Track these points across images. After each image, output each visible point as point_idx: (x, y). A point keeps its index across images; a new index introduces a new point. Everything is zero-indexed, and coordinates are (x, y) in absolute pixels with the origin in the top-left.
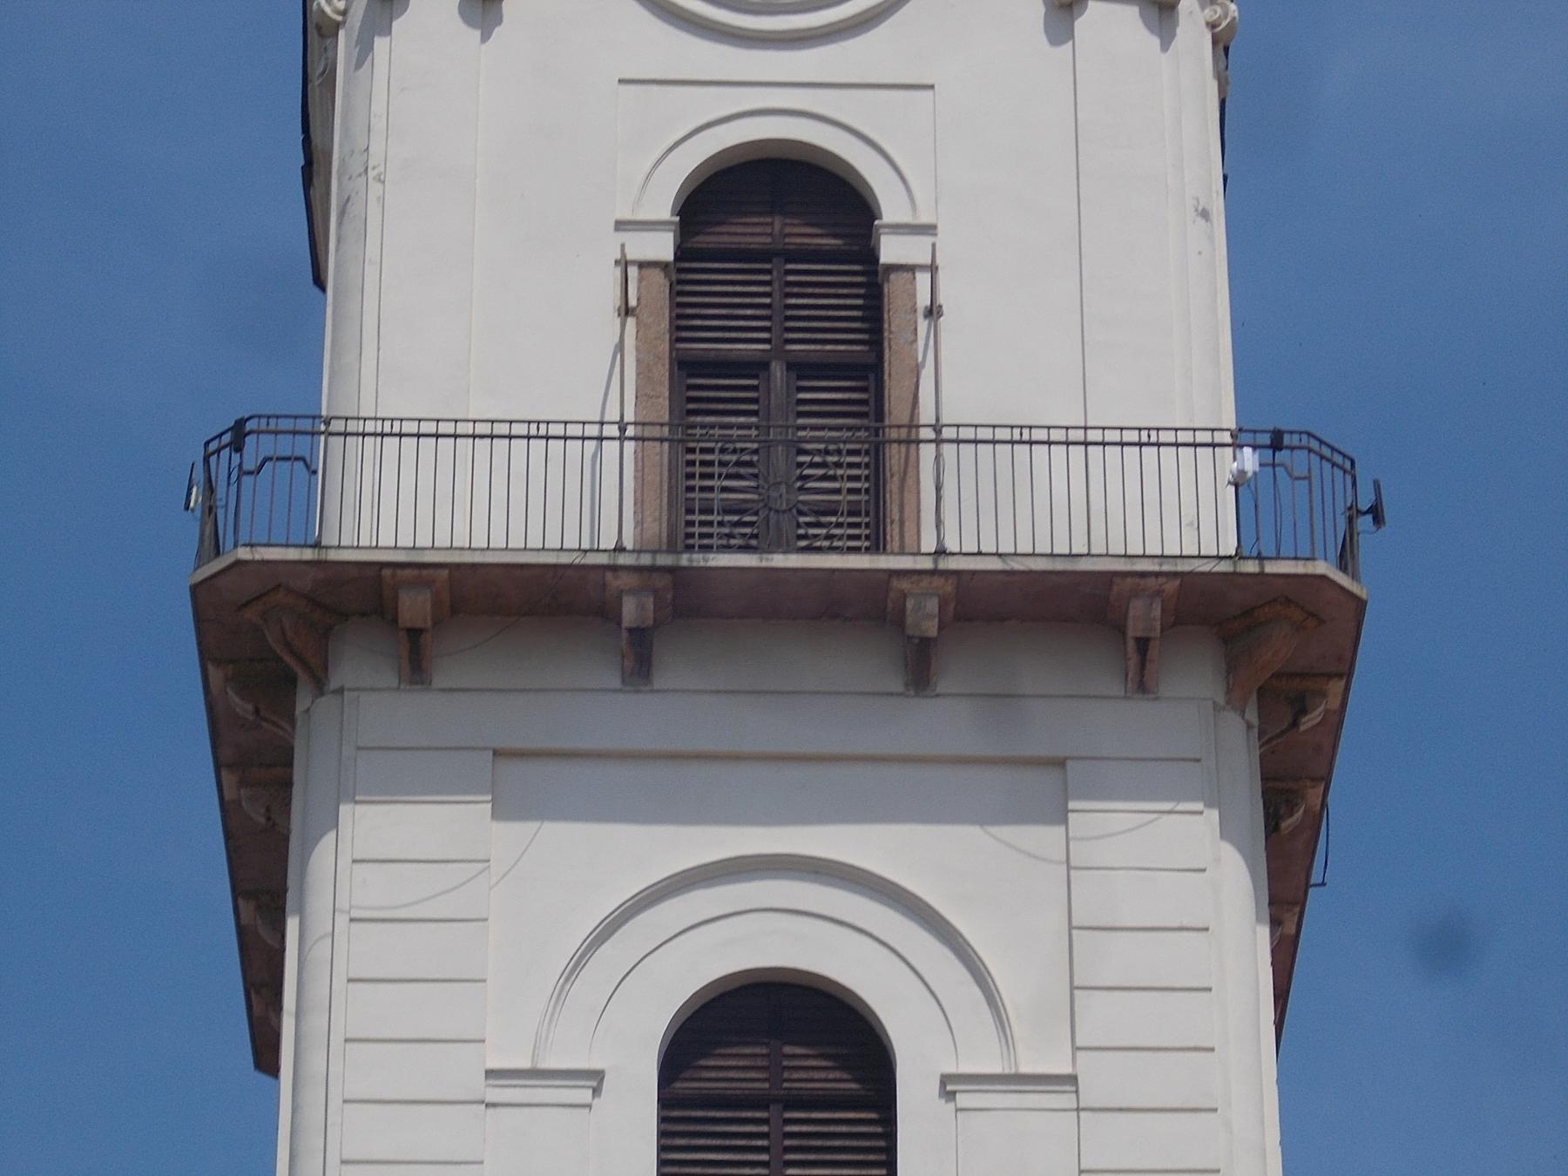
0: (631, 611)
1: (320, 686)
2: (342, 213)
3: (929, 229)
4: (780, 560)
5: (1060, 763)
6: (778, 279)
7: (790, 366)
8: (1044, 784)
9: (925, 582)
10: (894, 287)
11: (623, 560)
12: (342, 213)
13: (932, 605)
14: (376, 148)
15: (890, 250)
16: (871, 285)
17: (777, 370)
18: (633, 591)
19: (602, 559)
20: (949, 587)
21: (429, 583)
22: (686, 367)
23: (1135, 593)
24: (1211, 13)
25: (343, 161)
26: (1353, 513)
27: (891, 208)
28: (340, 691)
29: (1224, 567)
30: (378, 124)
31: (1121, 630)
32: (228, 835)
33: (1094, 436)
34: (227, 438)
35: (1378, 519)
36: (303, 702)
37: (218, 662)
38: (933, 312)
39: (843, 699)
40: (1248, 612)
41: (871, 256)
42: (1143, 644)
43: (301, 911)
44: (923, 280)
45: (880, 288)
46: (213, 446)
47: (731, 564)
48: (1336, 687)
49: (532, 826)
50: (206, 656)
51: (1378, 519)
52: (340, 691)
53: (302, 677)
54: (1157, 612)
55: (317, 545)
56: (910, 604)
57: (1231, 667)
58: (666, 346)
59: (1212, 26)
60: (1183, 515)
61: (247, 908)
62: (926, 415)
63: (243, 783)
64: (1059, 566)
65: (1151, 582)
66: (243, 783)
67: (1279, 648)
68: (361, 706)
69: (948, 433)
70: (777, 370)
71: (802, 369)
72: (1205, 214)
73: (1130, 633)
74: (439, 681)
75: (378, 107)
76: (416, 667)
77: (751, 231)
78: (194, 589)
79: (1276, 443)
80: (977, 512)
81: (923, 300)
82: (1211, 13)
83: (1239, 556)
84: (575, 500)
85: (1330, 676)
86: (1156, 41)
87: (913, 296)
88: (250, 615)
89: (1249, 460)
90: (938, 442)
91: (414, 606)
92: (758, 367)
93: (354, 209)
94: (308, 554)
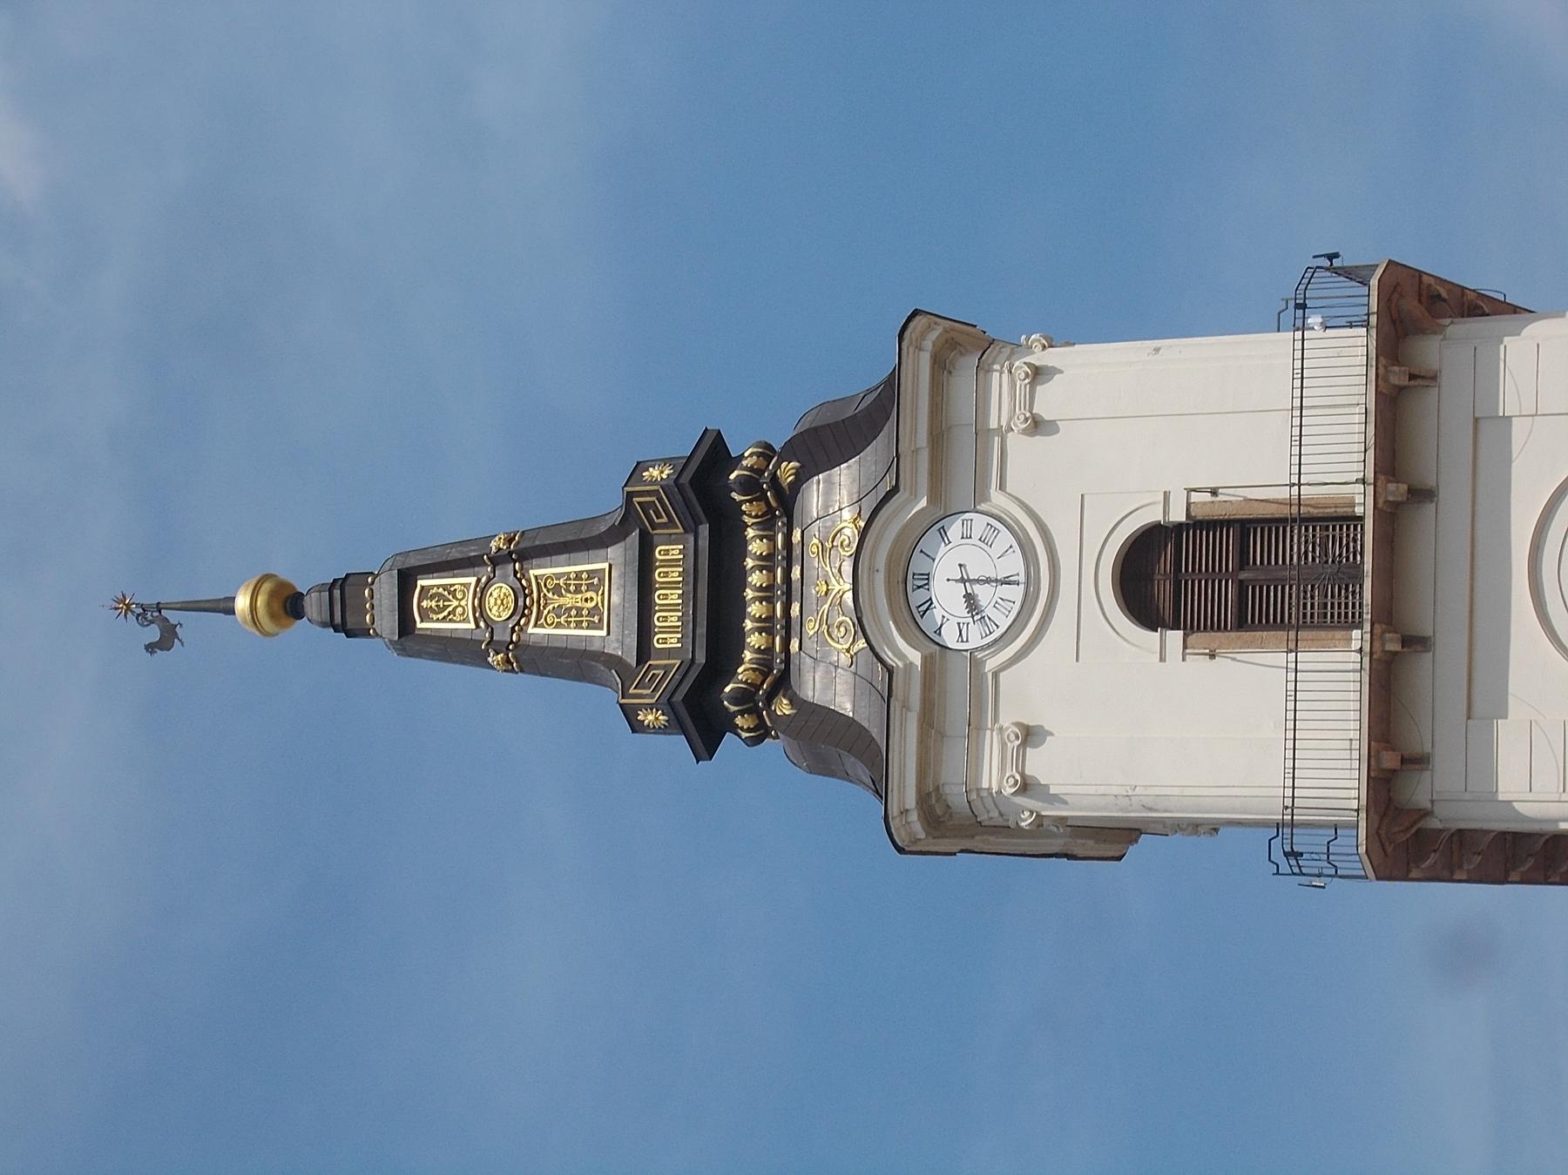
0: (1393, 646)
1: (1426, 814)
2: (1151, 809)
3: (1166, 495)
4: (1368, 566)
5: (1476, 420)
6: (1193, 575)
7: (1242, 568)
8: (1489, 428)
9: (1379, 490)
10: (1199, 513)
11: (1367, 648)
12: (1151, 809)
13: (1392, 487)
14: (1115, 790)
15: (1178, 515)
16: (1197, 525)
17: (1243, 575)
18: (1383, 645)
19: (1366, 660)
20: (1382, 477)
21: (1378, 752)
22: (1241, 624)
23: (1386, 380)
24: (1037, 348)
25: (1121, 810)
26: (1330, 269)
27: (1155, 515)
28: (1432, 802)
29: (1374, 332)
30: (1102, 790)
31: (1401, 389)
32: (1481, 882)
33: (1297, 403)
34: (1293, 862)
35: (1336, 255)
36: (1434, 824)
37: (1408, 871)
38: (1214, 492)
39: (1441, 532)
40: (1394, 322)
41: (1179, 526)
42: (1412, 377)
43: (1557, 821)
44: (1195, 497)
45: (1201, 522)
46: (1296, 870)
47: (914, 759)
48: (1425, 277)
49: (1511, 700)
50: (1406, 878)
51: (1336, 255)
52: (1432, 802)
53: (1419, 825)
54: (1396, 369)
55: (1357, 810)
56: (1391, 498)
57: (1422, 331)
58: (1233, 634)
59: (1044, 347)
60: (1344, 357)
61: (1514, 876)
62: (1283, 494)
63: (1460, 867)
64: (1372, 419)
65: (1381, 370)
66: (1460, 867)
67: (1411, 305)
68: (1444, 794)
69: (1295, 480)
70: (1243, 575)
71: (1243, 562)
72: (1157, 350)
73: (1406, 383)
74: (1428, 748)
75: (1092, 790)
76: (1417, 761)
77: (1163, 592)
78: (1378, 879)
79: (1303, 307)
80: (1338, 467)
81: (1207, 497)
82: (1037, 348)
83: (1367, 325)
84: (1335, 673)
85: (1420, 282)
86: (1057, 376)
87: (1205, 503)
88: (1389, 850)
89: (1314, 320)
90: (1300, 485)
91: (1390, 760)
92: (1242, 587)
93: (1149, 802)
94: (1363, 815)
